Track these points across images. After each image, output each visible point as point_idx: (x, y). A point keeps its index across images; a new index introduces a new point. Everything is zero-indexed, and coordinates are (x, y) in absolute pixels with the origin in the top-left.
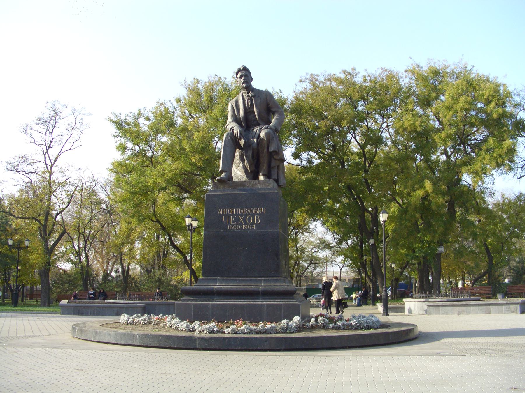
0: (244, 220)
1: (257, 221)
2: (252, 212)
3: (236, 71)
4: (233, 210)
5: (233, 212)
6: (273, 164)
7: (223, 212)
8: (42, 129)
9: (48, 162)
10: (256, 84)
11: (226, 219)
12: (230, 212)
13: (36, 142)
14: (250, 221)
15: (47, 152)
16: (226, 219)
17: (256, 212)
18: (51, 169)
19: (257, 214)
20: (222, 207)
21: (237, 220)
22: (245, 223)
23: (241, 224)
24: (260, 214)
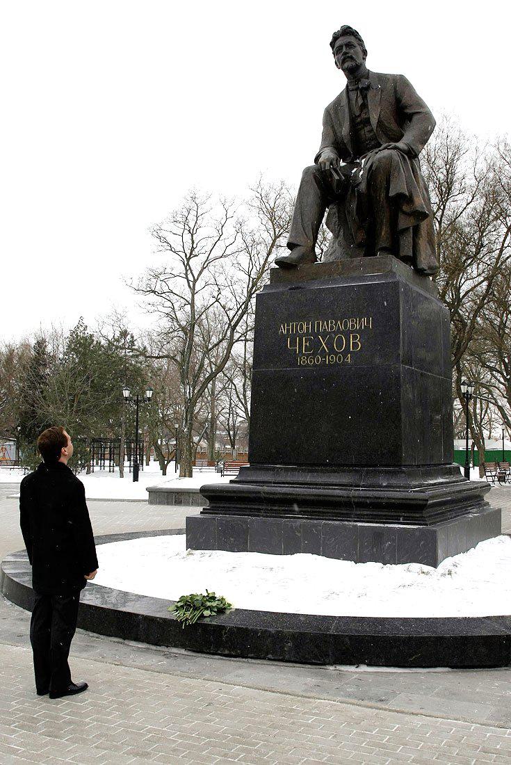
0: (329, 344)
1: (355, 345)
2: (346, 326)
3: (330, 39)
4: (308, 324)
5: (308, 328)
6: (404, 222)
7: (288, 330)
8: (178, 229)
9: (190, 278)
10: (374, 64)
11: (293, 343)
12: (301, 328)
13: (173, 250)
14: (340, 346)
15: (188, 264)
16: (293, 343)
17: (353, 326)
18: (194, 285)
19: (356, 331)
20: (288, 320)
21: (315, 346)
22: (332, 351)
23: (323, 354)
24: (360, 331)
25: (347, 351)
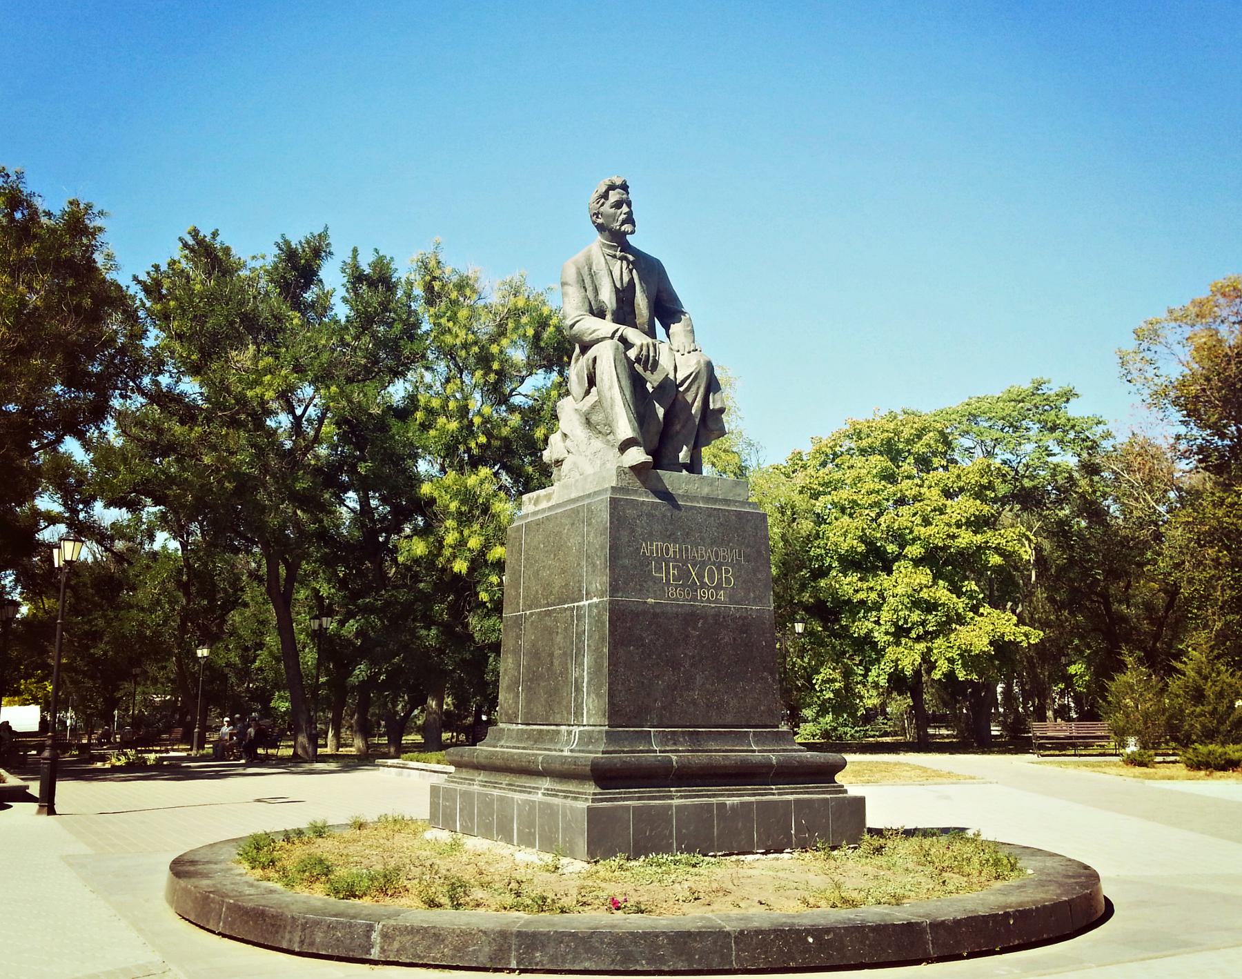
0: (700, 577)
11: (659, 570)
22: (703, 585)
25: (718, 587)
